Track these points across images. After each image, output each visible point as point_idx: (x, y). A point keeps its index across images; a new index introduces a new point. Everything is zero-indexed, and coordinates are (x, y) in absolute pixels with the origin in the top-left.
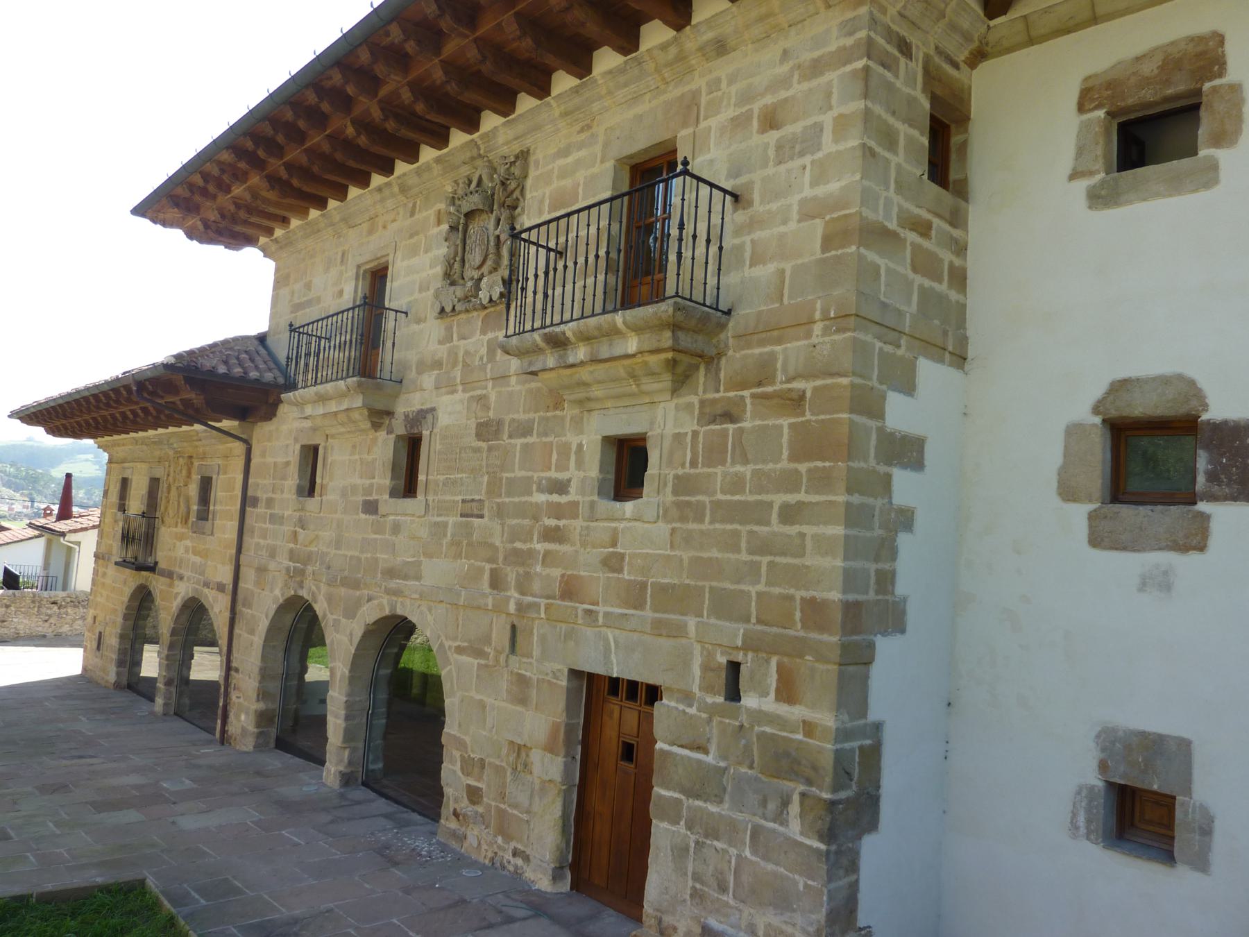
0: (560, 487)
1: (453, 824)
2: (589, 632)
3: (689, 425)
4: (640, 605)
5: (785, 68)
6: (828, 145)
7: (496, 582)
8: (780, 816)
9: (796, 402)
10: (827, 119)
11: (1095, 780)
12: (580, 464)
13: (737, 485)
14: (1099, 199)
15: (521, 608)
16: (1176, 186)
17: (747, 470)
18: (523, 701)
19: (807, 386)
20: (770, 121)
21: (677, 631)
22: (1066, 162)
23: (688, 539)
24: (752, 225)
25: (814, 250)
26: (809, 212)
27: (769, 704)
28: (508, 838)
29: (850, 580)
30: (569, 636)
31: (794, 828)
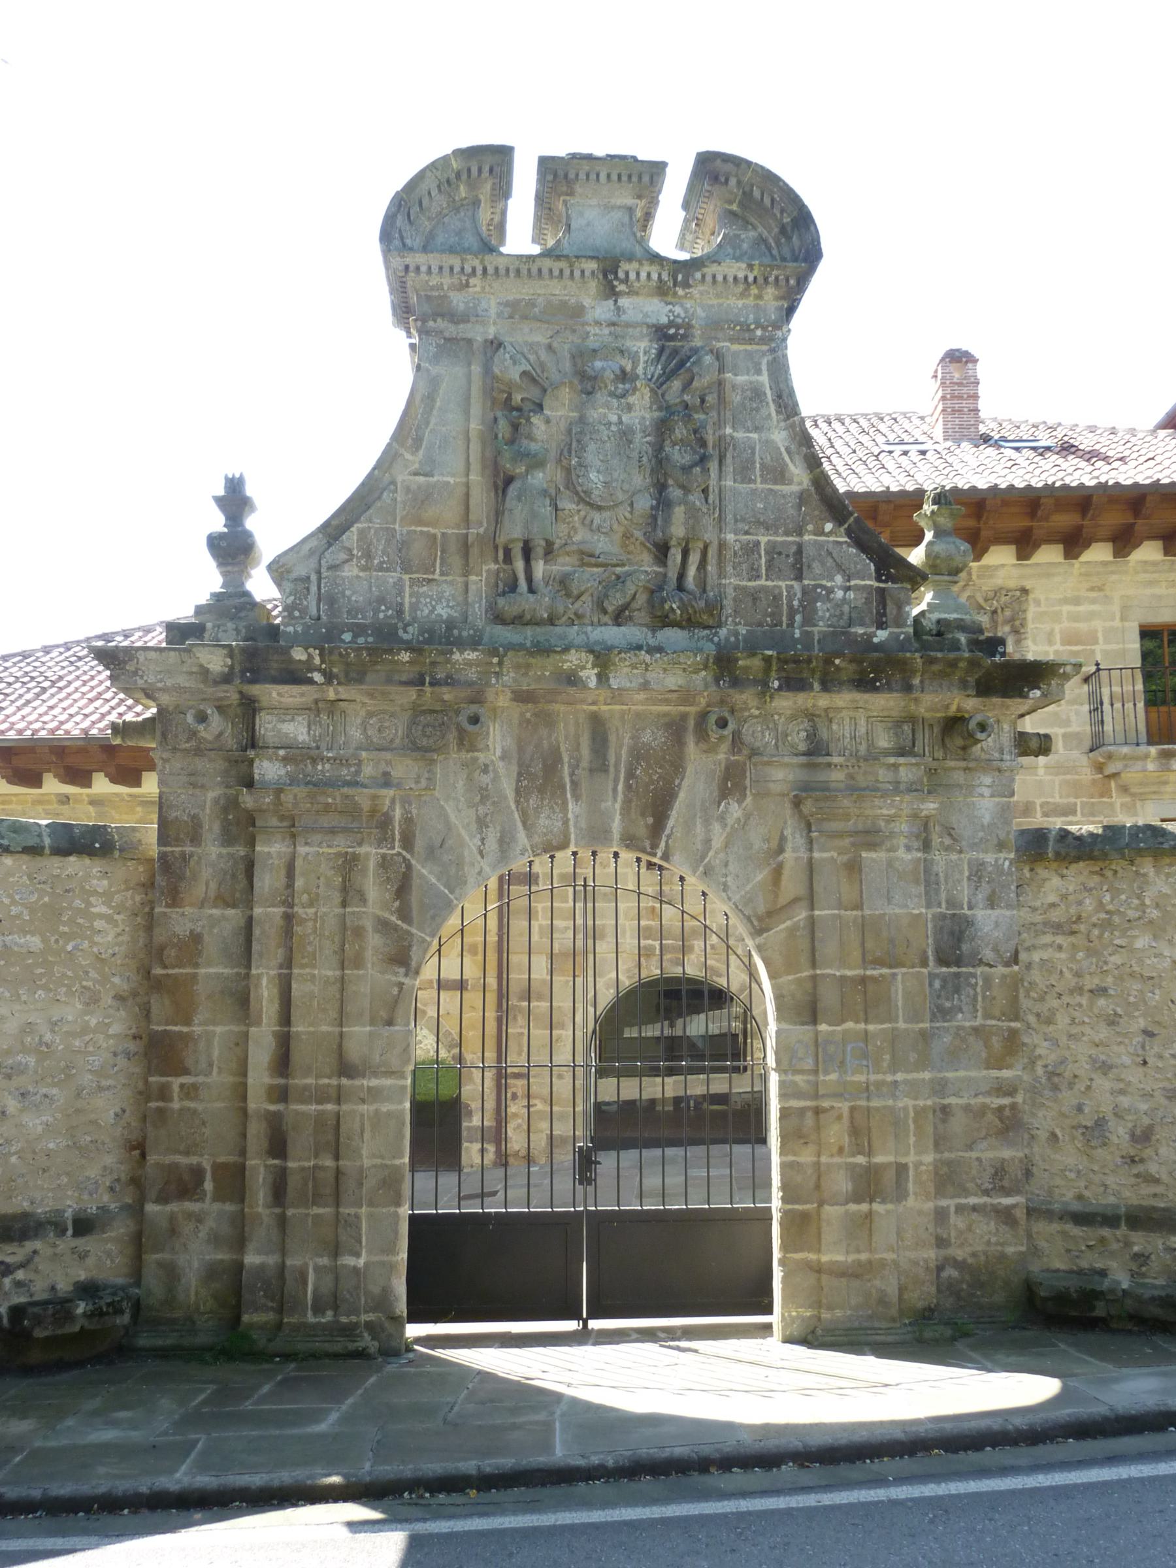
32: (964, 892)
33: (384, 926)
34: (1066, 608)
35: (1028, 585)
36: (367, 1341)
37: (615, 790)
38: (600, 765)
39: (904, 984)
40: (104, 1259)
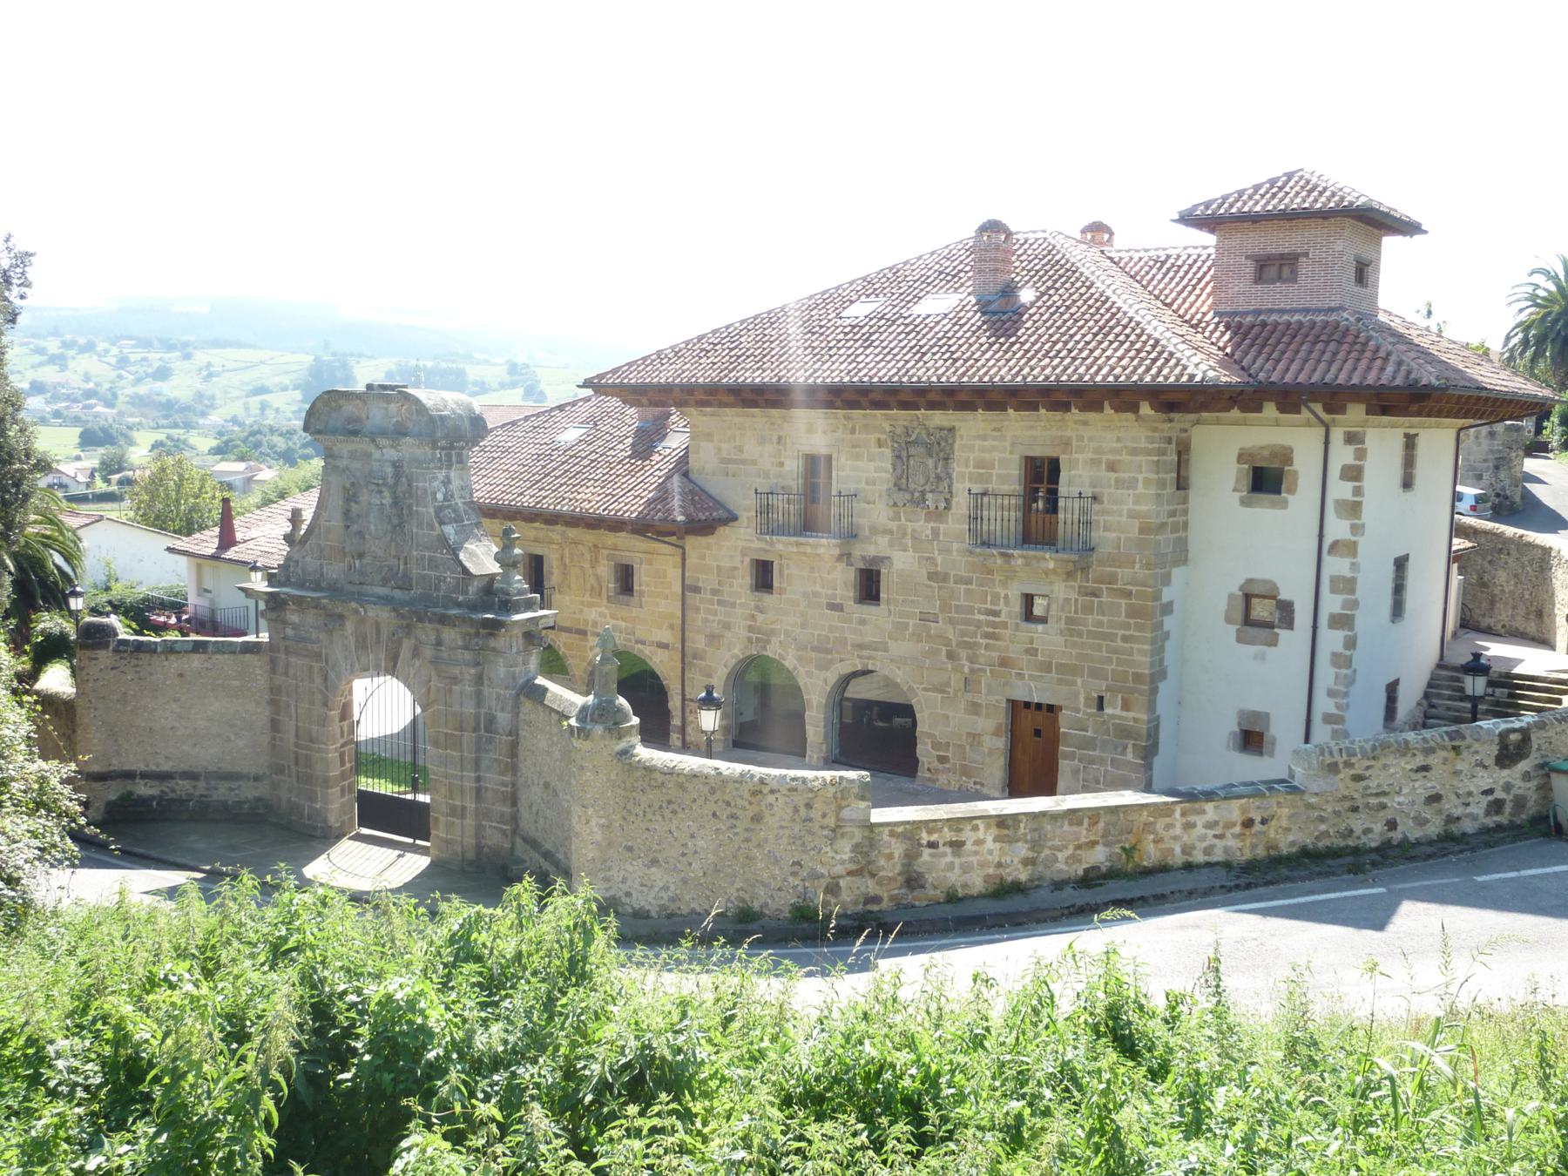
0: (996, 614)
1: (928, 775)
2: (1020, 683)
3: (1073, 596)
4: (1050, 671)
5: (1119, 445)
6: (1140, 489)
7: (951, 656)
8: (1124, 752)
9: (1129, 594)
10: (1141, 477)
11: (1236, 729)
12: (1007, 603)
13: (1100, 624)
14: (1245, 503)
15: (972, 671)
16: (1273, 505)
17: (1105, 619)
18: (977, 714)
19: (1134, 589)
20: (1112, 467)
21: (1074, 683)
22: (1232, 483)
23: (1075, 645)
24: (1103, 512)
25: (1135, 533)
26: (1132, 515)
27: (1118, 712)
28: (969, 776)
29: (1152, 665)
30: (1005, 684)
31: (1130, 756)
32: (494, 704)
33: (321, 692)
34: (978, 443)
35: (956, 424)
36: (318, 833)
37: (1521, 310)
38: (378, 641)
39: (468, 738)
40: (262, 790)
